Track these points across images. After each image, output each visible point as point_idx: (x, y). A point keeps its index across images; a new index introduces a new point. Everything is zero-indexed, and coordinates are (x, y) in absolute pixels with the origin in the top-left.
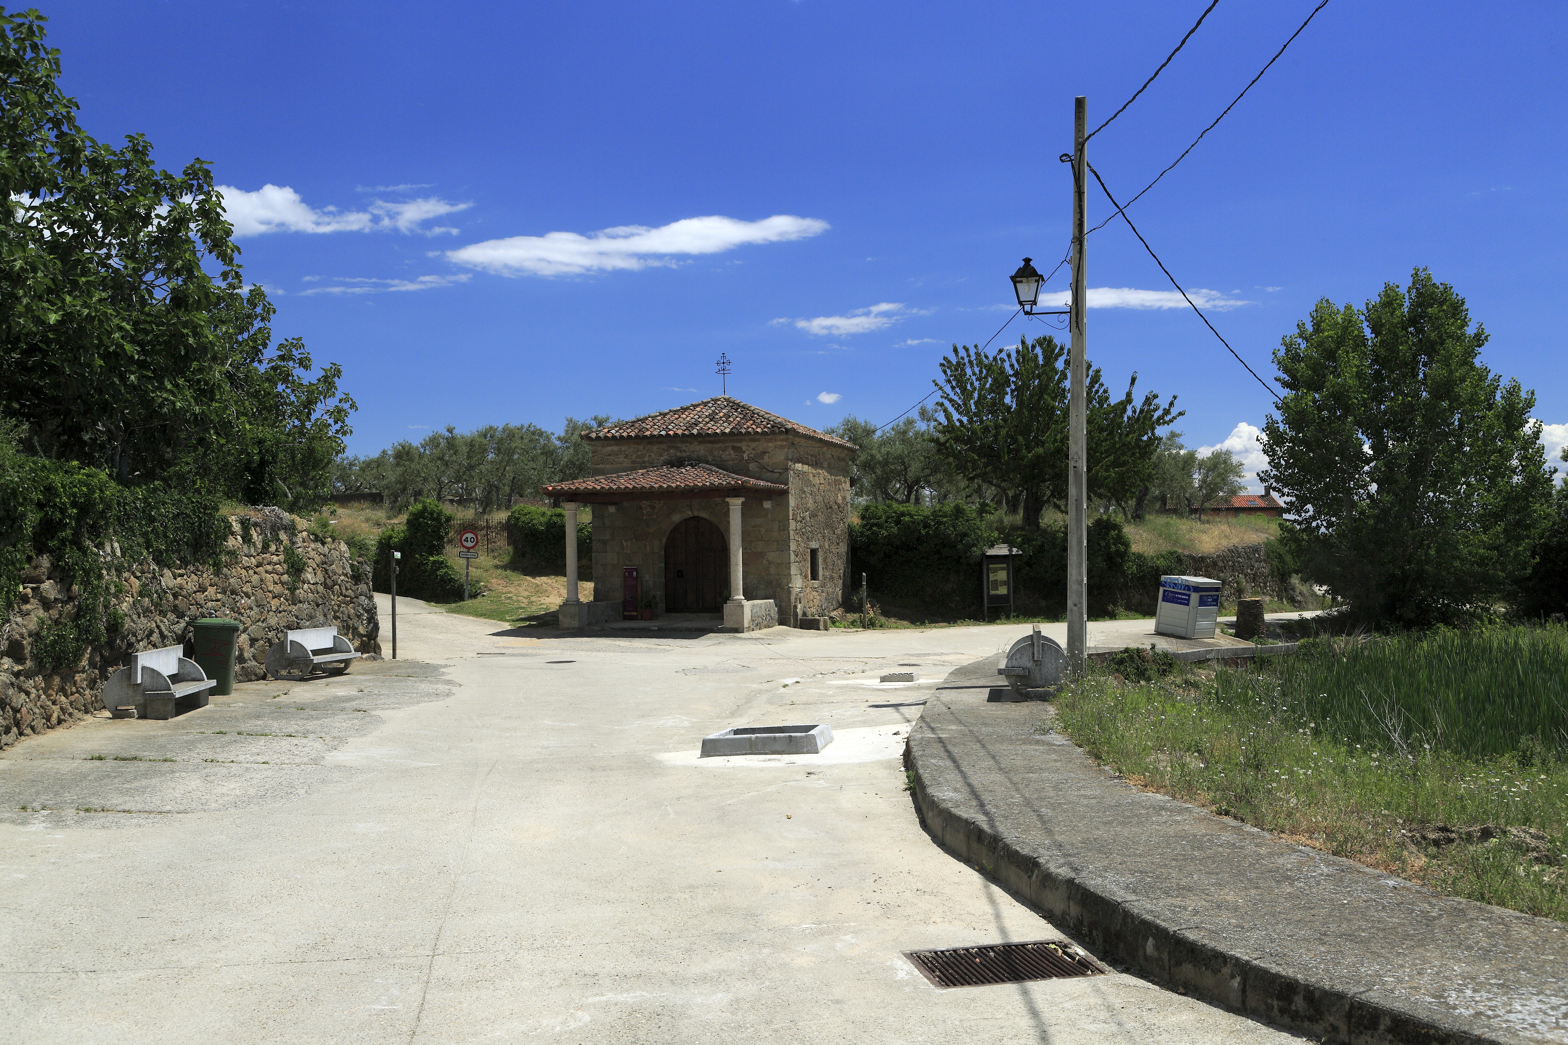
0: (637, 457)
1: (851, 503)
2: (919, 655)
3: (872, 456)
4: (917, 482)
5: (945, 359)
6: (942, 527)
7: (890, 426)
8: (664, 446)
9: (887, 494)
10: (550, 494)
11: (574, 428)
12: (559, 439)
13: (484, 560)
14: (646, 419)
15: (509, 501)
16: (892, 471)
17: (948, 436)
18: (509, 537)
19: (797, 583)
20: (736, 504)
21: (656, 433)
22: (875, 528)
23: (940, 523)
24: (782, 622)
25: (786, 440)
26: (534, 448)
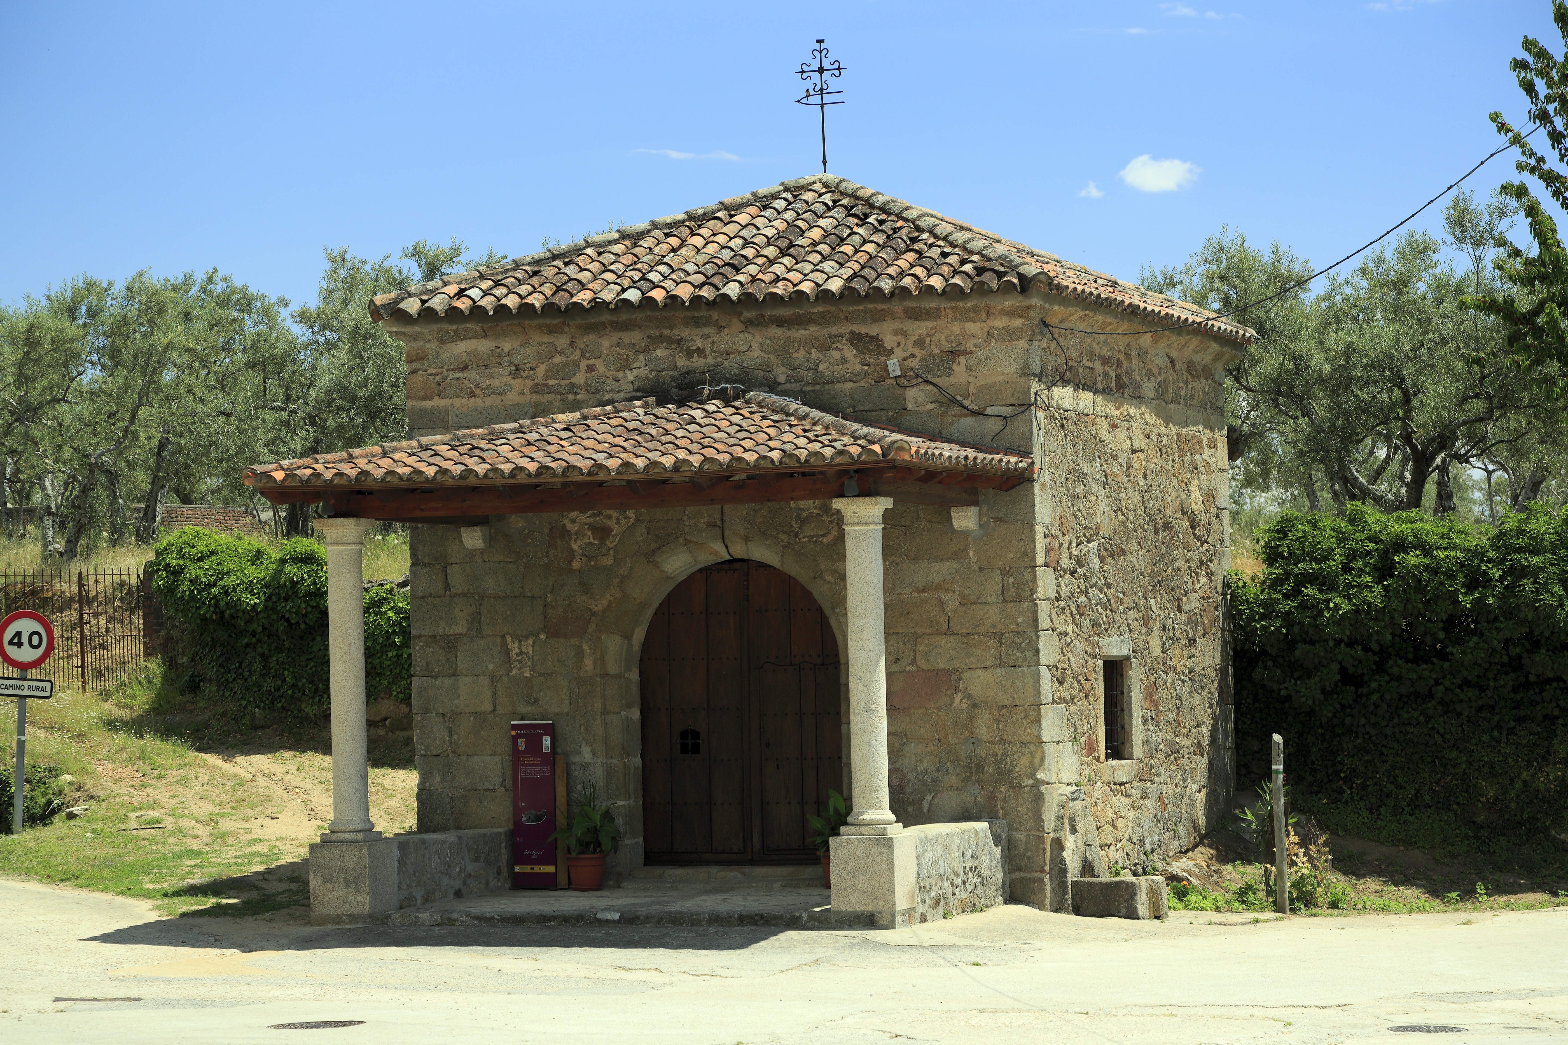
0: (552, 373)
1: (1236, 514)
2: (1457, 997)
3: (1296, 358)
4: (1444, 441)
5: (1528, 44)
6: (1527, 584)
7: (1356, 263)
8: (635, 337)
9: (1347, 480)
10: (277, 494)
11: (351, 283)
12: (304, 317)
13: (73, 701)
14: (579, 251)
15: (149, 514)
16: (1363, 408)
17: (1542, 290)
18: (149, 630)
19: (1064, 766)
20: (864, 520)
21: (608, 295)
22: (1310, 591)
23: (1518, 572)
24: (1016, 893)
25: (1023, 312)
26: (226, 347)
